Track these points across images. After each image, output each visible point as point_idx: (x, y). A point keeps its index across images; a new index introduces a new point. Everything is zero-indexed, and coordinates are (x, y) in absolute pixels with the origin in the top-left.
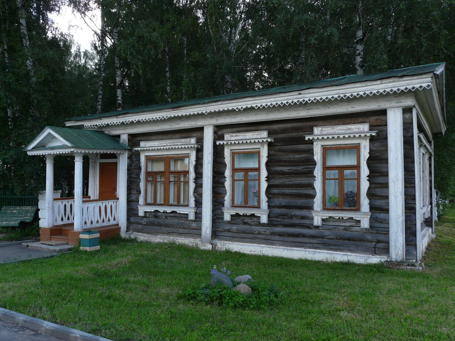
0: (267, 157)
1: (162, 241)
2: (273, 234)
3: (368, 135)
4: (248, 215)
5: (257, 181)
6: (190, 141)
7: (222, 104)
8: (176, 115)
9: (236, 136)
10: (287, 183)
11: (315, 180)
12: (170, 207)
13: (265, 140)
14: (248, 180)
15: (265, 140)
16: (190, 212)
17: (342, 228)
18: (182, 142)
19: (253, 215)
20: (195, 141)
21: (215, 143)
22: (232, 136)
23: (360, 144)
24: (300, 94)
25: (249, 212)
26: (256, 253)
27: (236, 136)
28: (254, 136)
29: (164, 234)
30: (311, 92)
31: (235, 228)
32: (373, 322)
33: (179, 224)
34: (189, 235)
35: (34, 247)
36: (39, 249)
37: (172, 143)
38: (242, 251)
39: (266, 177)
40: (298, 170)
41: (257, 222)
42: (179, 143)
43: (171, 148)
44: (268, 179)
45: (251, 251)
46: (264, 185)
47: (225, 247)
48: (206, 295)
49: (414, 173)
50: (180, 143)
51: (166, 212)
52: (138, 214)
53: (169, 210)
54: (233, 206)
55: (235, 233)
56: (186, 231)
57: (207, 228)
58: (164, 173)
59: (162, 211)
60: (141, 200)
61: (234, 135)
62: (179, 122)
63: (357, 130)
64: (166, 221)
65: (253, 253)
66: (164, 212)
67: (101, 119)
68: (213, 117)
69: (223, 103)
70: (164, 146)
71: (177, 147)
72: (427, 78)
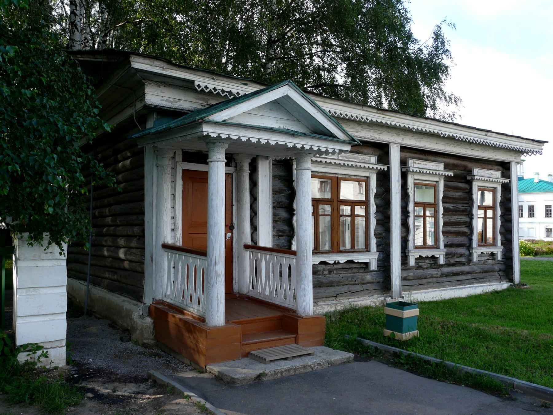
0: (443, 192)
1: (333, 309)
2: (442, 275)
6: (369, 160)
7: (430, 124)
9: (419, 163)
10: (452, 220)
12: (341, 254)
13: (499, 180)
14: (341, 216)
17: (483, 262)
18: (359, 159)
21: (401, 170)
22: (415, 163)
24: (486, 135)
26: (437, 299)
27: (419, 163)
28: (433, 167)
29: (328, 299)
30: (493, 136)
31: (412, 274)
33: (350, 279)
34: (365, 292)
35: (282, 372)
36: (302, 370)
37: (346, 157)
38: (426, 300)
40: (458, 208)
41: (429, 265)
42: (356, 159)
43: (350, 165)
45: (433, 298)
47: (409, 298)
50: (357, 159)
51: (339, 263)
53: (342, 259)
54: (316, 251)
55: (411, 280)
56: (358, 288)
57: (396, 278)
58: (331, 201)
59: (332, 262)
61: (417, 162)
62: (359, 128)
63: (495, 176)
64: (329, 277)
65: (435, 299)
66: (335, 263)
67: (246, 85)
68: (399, 135)
69: (432, 123)
70: (345, 161)
71: (350, 163)
72: (525, 143)
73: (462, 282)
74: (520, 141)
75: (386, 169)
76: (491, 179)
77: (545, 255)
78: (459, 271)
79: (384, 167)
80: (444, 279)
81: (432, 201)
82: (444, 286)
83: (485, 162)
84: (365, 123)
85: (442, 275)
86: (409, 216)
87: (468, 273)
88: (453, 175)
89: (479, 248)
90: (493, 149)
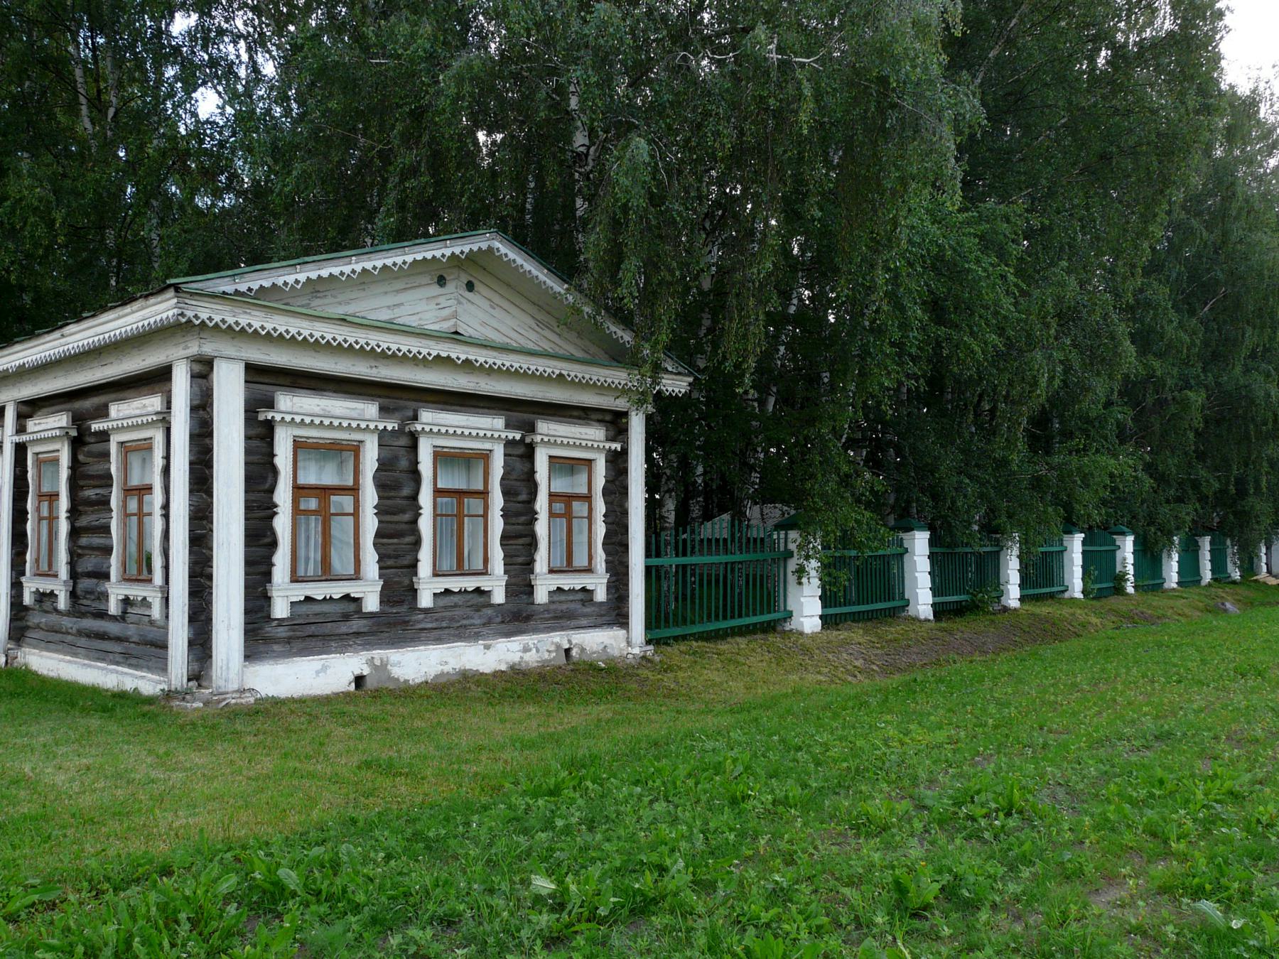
2: (80, 633)
3: (503, 436)
4: (336, 597)
5: (439, 512)
8: (444, 354)
11: (375, 507)
13: (601, 445)
15: (372, 426)
16: (599, 586)
19: (347, 597)
20: (162, 404)
23: (490, 451)
25: (470, 583)
32: (1088, 688)
39: (375, 507)
44: (381, 511)
46: (370, 524)
48: (200, 921)
49: (253, 497)
52: (269, 616)
60: (541, 564)
72: (133, 312)
73: (102, 656)
74: (121, 313)
75: (619, 449)
76: (552, 440)
77: (1050, 602)
78: (102, 630)
79: (617, 446)
80: (83, 641)
81: (584, 490)
82: (75, 655)
83: (575, 413)
84: (81, 354)
85: (80, 633)
86: (68, 511)
87: (119, 639)
88: (619, 449)
89: (550, 576)
90: (489, 375)
